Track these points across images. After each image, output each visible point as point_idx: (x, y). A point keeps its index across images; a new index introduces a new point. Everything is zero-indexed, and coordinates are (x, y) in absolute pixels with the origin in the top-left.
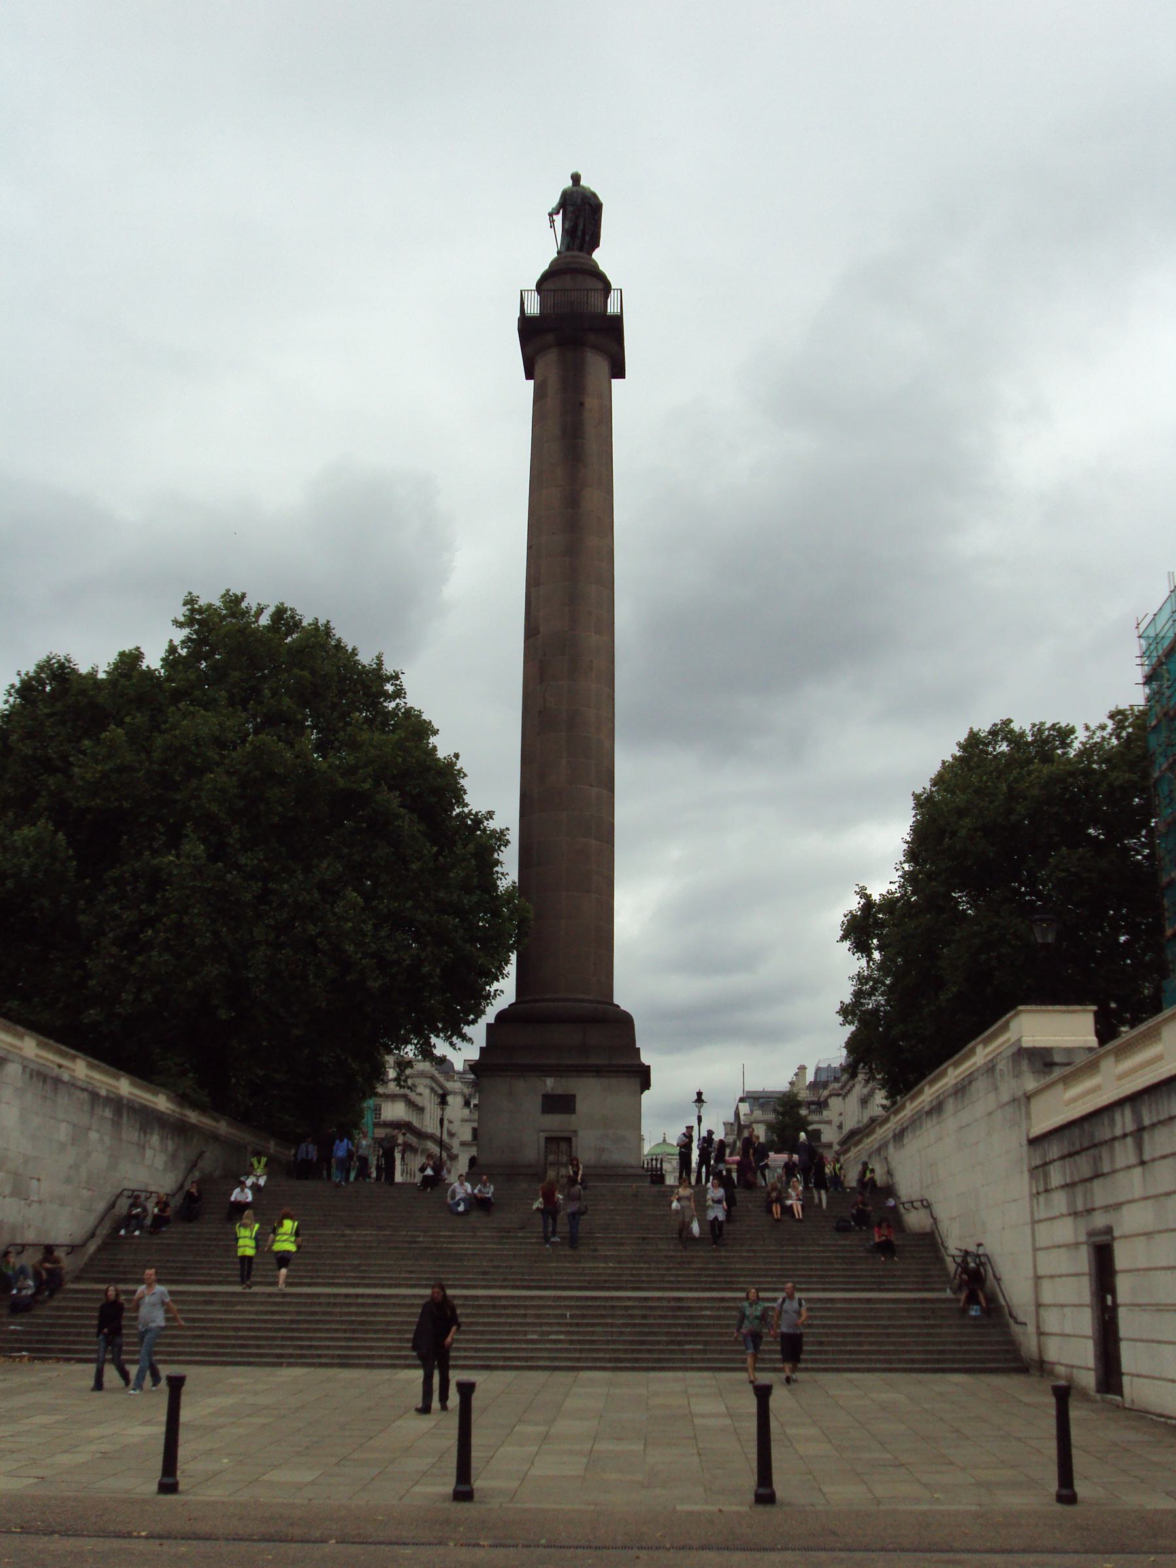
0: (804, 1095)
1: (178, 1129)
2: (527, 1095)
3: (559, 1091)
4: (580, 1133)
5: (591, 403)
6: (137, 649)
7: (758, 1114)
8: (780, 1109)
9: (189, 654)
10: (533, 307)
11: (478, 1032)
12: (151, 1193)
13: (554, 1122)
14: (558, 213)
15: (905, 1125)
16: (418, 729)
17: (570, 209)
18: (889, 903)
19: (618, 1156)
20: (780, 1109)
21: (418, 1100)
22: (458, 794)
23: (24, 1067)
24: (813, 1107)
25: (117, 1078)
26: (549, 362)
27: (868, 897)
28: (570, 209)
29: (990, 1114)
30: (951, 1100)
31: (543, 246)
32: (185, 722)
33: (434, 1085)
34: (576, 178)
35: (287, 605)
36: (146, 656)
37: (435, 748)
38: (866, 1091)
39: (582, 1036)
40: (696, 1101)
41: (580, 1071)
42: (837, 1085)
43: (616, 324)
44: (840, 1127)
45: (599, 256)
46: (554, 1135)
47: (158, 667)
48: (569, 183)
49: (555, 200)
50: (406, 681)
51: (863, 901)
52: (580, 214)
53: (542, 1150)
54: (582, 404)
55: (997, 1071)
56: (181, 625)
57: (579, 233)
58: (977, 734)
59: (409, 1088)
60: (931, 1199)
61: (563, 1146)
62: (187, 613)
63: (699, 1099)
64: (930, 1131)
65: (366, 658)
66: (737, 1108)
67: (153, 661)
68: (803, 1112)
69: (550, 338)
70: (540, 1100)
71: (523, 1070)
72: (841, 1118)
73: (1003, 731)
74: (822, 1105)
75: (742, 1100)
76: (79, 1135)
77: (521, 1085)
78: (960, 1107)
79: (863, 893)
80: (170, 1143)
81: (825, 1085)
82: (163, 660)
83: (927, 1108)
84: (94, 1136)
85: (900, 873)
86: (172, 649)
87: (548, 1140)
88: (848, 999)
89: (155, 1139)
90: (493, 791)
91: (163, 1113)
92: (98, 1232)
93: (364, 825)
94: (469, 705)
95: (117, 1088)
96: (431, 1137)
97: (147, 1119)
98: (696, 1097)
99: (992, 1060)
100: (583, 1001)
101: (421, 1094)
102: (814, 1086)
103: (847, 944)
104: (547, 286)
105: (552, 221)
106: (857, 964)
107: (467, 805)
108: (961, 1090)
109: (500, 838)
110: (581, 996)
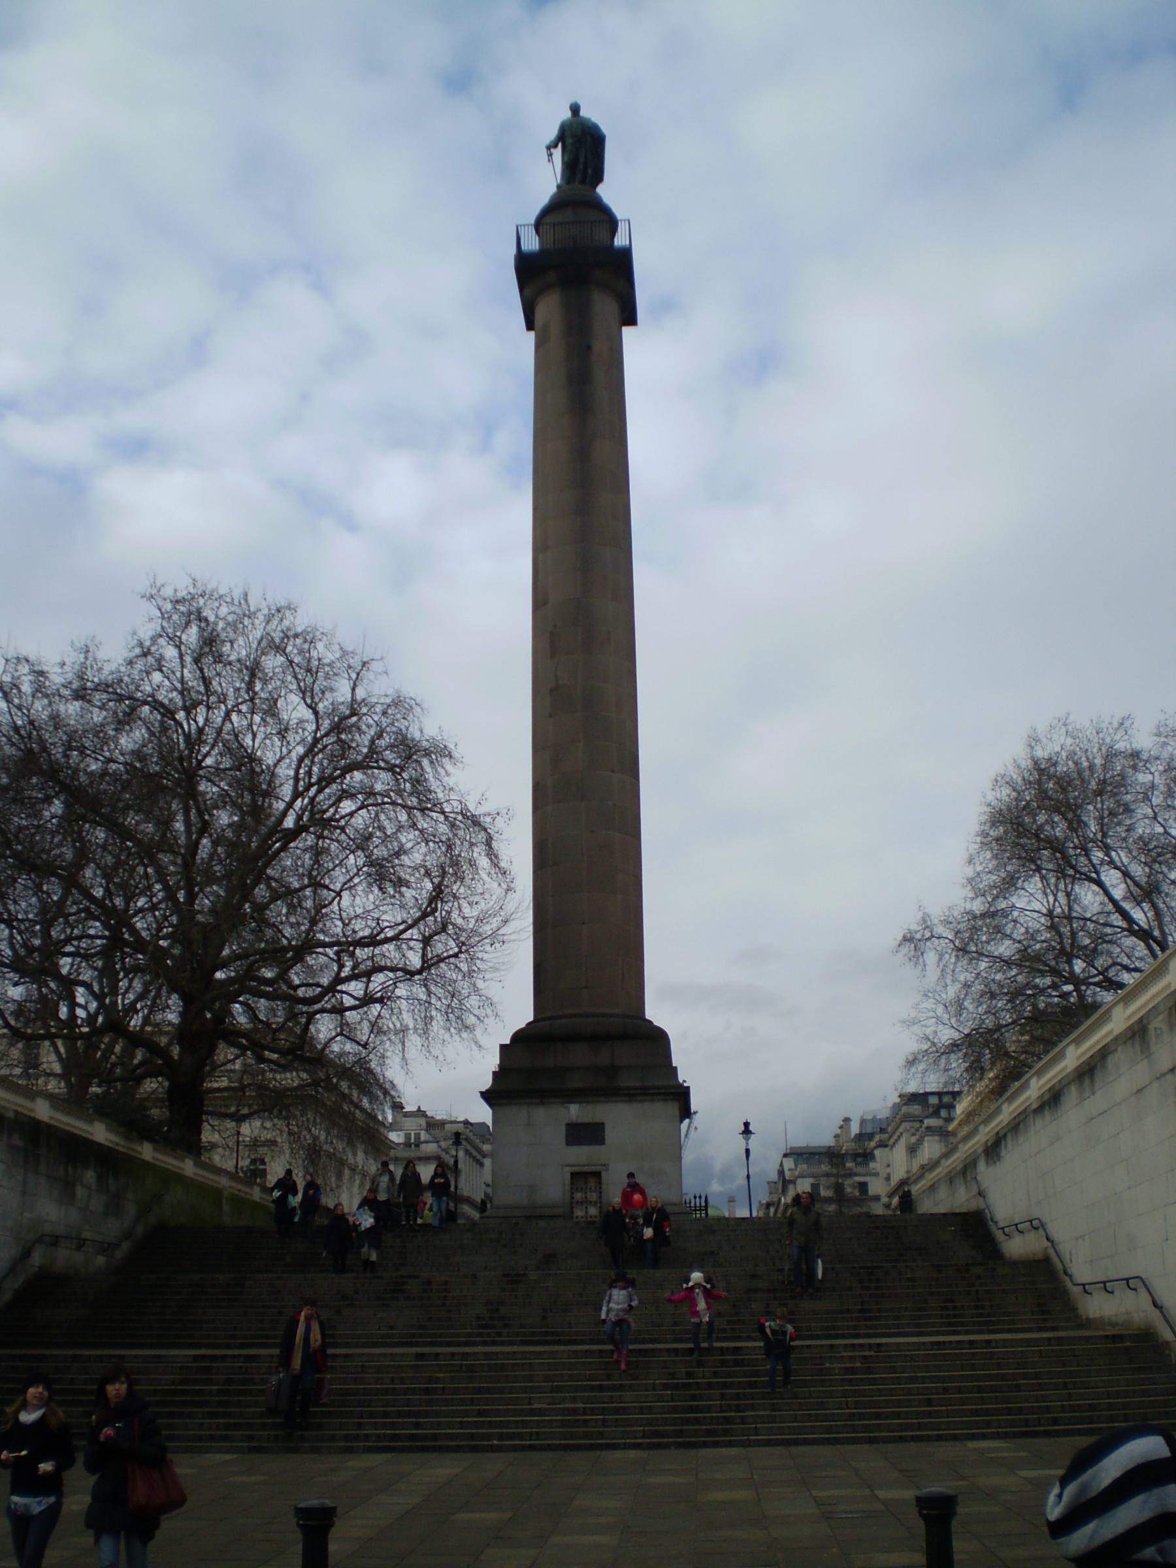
3: (586, 1120)
5: (599, 347)
10: (532, 243)
13: (581, 1155)
14: (556, 146)
15: (1001, 1134)
17: (569, 141)
24: (859, 1159)
26: (549, 306)
28: (569, 141)
29: (1140, 1091)
30: (1073, 1088)
31: (544, 179)
34: (575, 109)
38: (913, 1139)
39: (593, 1042)
42: (884, 1136)
43: (624, 258)
44: (888, 1178)
46: (576, 1169)
49: (553, 133)
52: (582, 147)
53: (568, 1188)
54: (589, 348)
55: (1151, 1032)
57: (581, 167)
61: (592, 1182)
63: (747, 1131)
64: (1040, 1131)
66: (781, 1164)
70: (563, 1130)
72: (888, 1170)
74: (868, 1156)
75: (785, 1155)
77: (541, 1114)
78: (1087, 1094)
81: (871, 1136)
83: (1035, 1106)
91: (100, 1145)
99: (1141, 1020)
100: (612, 1016)
102: (860, 1137)
105: (550, 155)
108: (1088, 1072)
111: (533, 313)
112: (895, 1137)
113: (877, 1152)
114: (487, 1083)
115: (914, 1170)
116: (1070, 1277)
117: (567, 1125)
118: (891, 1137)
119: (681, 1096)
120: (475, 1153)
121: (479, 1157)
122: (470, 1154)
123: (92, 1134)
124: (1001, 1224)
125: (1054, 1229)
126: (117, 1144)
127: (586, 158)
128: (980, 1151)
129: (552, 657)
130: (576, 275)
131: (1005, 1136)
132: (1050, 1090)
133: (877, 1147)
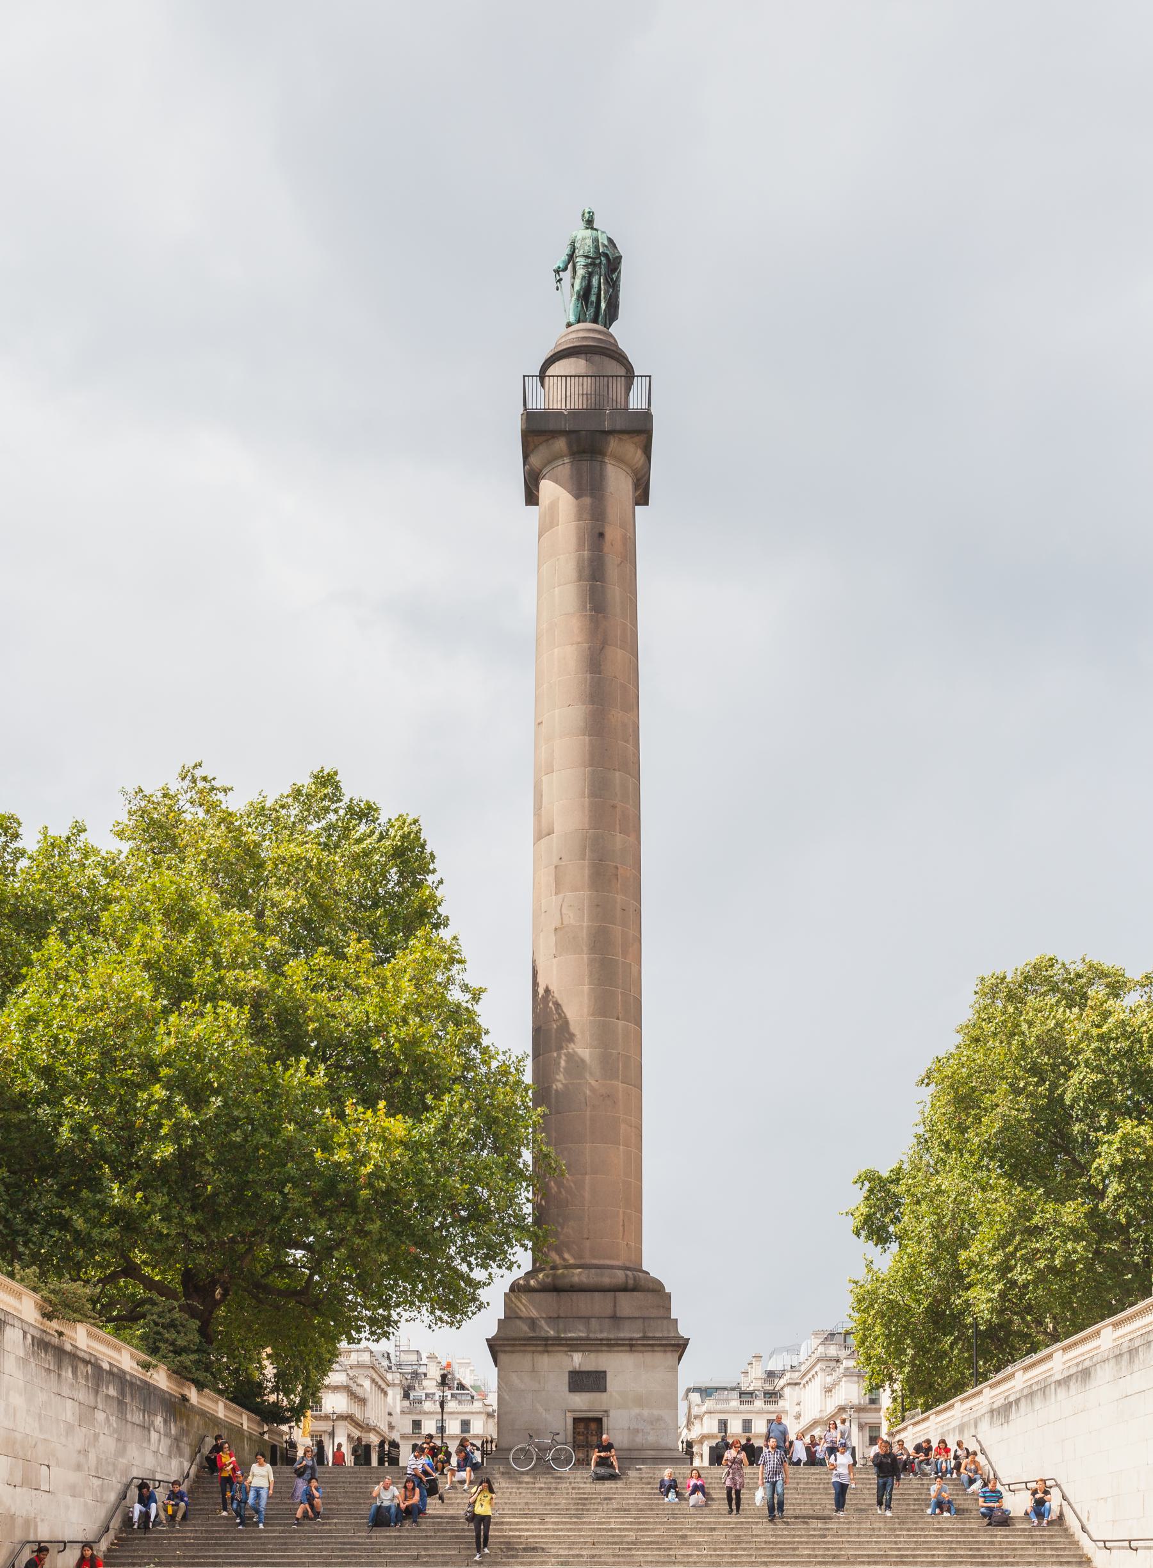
1: (176, 1408)
2: (555, 1369)
4: (612, 1413)
12: (160, 1481)
13: (582, 1402)
17: (581, 262)
19: (666, 1442)
21: (359, 1391)
23: (25, 1333)
31: (555, 317)
33: (375, 1376)
38: (829, 1379)
41: (610, 1345)
44: (798, 1417)
52: (232, 789)
54: (601, 535)
57: (593, 298)
61: (593, 1426)
64: (1062, 1402)
69: (561, 444)
71: (548, 1345)
76: (86, 1415)
77: (545, 1361)
83: (1058, 1377)
84: (100, 1416)
87: (576, 1421)
89: (159, 1421)
92: (111, 1526)
110: (601, 1262)
113: (787, 1390)
114: (492, 1331)
117: (570, 1372)
119: (679, 1346)
120: (380, 1382)
121: (383, 1386)
129: (556, 894)
130: (589, 443)
132: (1077, 1365)
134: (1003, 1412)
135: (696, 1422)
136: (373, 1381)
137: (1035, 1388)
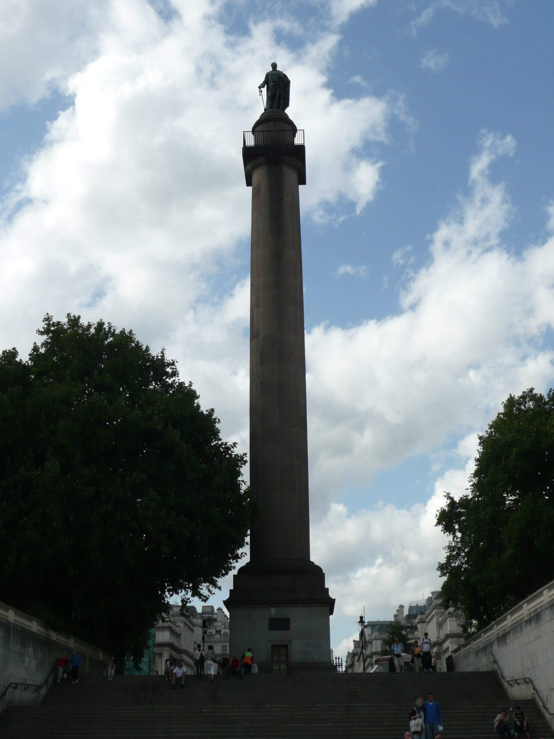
0: (403, 623)
1: (45, 644)
6: (14, 349)
7: (376, 634)
8: (390, 631)
9: (46, 351)
10: (251, 142)
11: (226, 583)
12: (28, 685)
13: (277, 636)
14: (264, 87)
15: (507, 631)
16: (187, 395)
18: (464, 502)
20: (390, 631)
21: (177, 630)
22: (215, 434)
24: (408, 630)
25: (7, 610)
27: (452, 499)
28: (271, 84)
31: (258, 105)
32: (45, 389)
34: (274, 66)
35: (106, 321)
36: (19, 354)
37: (198, 406)
38: (441, 619)
39: (292, 585)
40: (360, 622)
45: (288, 111)
47: (28, 360)
48: (270, 69)
49: (262, 79)
50: (179, 367)
51: (449, 501)
56: (42, 333)
57: (277, 98)
58: (514, 398)
59: (172, 623)
60: (533, 678)
61: (283, 650)
62: (46, 326)
64: (529, 633)
65: (155, 352)
67: (24, 357)
68: (404, 632)
69: (261, 159)
73: (529, 395)
74: (414, 628)
79: (448, 496)
80: (40, 653)
82: (30, 355)
83: (526, 619)
85: (471, 483)
86: (36, 349)
88: (443, 561)
89: (30, 650)
90: (236, 436)
91: (35, 633)
93: (158, 452)
94: (219, 380)
95: (7, 617)
96: (186, 652)
97: (26, 637)
98: (359, 620)
101: (178, 627)
102: (409, 617)
103: (440, 527)
104: (256, 130)
106: (448, 539)
107: (220, 440)
109: (240, 460)
111: (251, 178)
112: (430, 617)
113: (419, 626)
115: (441, 637)
116: (547, 709)
117: (270, 619)
118: (427, 617)
120: (189, 624)
121: (191, 626)
122: (187, 625)
123: (31, 627)
124: (508, 679)
125: (537, 683)
126: (42, 632)
127: (280, 94)
128: (494, 638)
131: (509, 632)
132: (534, 611)
133: (419, 623)
134: (502, 638)
135: (369, 645)
136: (185, 624)
137: (516, 625)
